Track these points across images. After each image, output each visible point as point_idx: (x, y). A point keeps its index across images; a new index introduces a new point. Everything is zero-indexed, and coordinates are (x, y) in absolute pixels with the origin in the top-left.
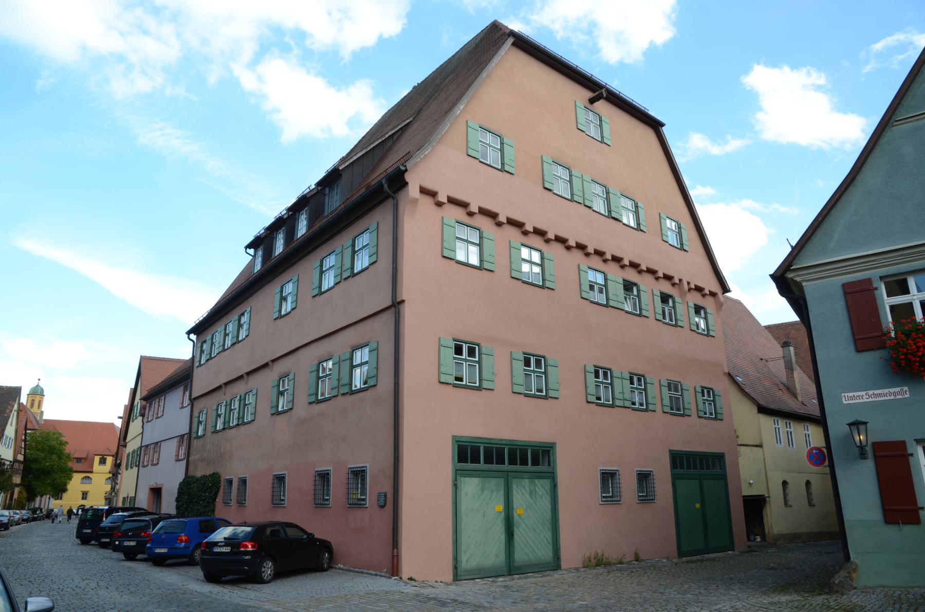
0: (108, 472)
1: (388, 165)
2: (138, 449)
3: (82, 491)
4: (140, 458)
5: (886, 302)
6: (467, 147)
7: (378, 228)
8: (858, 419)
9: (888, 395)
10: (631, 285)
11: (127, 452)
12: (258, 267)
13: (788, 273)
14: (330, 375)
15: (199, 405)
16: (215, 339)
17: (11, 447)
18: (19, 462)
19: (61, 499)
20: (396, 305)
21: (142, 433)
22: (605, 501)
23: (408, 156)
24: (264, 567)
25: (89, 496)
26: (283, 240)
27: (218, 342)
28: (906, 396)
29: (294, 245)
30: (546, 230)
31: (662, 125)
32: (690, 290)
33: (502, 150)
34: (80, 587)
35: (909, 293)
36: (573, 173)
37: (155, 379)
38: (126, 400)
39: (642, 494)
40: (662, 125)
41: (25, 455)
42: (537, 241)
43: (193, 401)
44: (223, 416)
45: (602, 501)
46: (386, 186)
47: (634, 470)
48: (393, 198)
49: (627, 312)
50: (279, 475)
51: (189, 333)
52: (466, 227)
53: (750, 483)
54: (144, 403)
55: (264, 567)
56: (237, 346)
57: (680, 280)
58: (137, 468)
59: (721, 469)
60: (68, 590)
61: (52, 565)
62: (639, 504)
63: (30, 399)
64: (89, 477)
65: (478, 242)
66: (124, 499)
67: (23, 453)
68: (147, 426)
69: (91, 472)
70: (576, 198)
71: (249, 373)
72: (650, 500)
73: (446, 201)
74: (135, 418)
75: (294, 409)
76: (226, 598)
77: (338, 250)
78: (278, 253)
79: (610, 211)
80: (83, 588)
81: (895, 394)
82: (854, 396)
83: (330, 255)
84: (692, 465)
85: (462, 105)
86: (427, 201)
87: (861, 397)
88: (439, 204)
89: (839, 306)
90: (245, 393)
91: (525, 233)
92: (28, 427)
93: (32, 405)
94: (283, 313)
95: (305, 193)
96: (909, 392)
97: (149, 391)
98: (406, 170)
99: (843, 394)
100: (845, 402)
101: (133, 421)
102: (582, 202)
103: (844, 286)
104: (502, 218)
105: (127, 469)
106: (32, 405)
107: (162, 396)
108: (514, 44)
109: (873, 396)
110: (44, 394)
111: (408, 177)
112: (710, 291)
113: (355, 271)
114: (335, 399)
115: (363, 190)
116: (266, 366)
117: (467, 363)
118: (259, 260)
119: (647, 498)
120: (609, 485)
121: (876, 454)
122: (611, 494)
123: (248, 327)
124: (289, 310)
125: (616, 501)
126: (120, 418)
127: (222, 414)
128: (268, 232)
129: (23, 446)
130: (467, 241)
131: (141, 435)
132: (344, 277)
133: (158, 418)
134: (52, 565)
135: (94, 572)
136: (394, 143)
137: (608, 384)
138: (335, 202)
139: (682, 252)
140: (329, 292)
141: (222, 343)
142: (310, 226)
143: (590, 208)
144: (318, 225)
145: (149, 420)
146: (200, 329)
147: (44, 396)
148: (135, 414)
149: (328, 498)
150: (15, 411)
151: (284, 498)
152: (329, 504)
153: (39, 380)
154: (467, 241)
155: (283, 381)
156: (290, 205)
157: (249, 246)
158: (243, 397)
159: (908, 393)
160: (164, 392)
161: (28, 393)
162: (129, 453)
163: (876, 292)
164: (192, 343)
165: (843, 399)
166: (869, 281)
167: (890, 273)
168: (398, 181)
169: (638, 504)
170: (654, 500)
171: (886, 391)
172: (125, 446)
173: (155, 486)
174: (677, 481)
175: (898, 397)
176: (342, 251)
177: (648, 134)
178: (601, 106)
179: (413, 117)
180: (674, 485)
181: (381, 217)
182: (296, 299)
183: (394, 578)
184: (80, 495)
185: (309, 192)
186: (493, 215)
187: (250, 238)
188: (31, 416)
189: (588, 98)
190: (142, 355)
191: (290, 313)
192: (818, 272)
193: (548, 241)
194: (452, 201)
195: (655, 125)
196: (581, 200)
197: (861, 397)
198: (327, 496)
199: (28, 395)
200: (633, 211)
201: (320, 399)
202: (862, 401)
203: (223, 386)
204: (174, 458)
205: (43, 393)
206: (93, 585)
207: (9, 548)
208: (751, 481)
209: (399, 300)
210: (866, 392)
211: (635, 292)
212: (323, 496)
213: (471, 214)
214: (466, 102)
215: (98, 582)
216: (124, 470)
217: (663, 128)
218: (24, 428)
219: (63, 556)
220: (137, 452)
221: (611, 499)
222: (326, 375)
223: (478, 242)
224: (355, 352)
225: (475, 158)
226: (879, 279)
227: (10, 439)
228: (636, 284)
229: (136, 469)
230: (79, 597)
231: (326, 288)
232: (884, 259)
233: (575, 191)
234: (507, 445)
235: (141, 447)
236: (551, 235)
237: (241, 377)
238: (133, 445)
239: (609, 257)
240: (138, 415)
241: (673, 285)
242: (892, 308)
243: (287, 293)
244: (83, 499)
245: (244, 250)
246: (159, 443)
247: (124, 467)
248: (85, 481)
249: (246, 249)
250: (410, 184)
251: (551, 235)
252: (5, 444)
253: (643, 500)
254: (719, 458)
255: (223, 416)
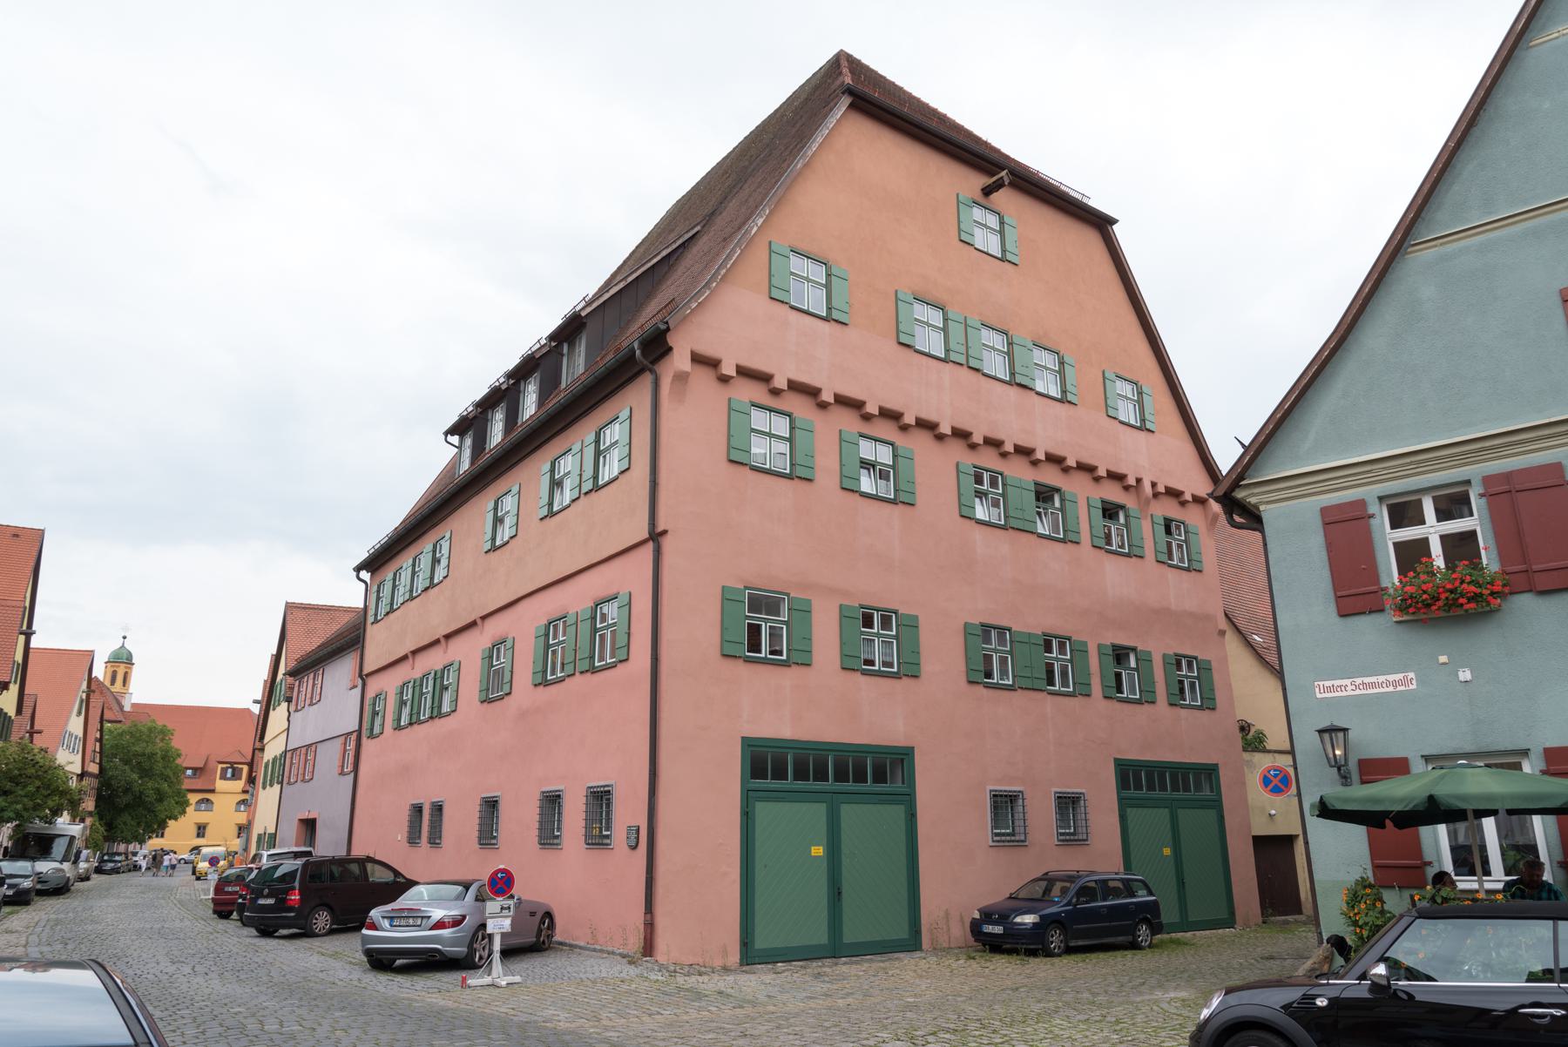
0: (240, 790)
1: (647, 317)
2: (281, 755)
3: (196, 823)
4: (284, 769)
5: (1388, 537)
6: (770, 285)
7: (631, 417)
8: (1335, 724)
9: (1384, 685)
10: (1049, 491)
11: (265, 760)
12: (465, 465)
13: (1237, 490)
14: (614, 624)
15: (374, 686)
16: (419, 566)
17: (78, 751)
18: (91, 775)
19: (162, 836)
20: (656, 536)
21: (288, 729)
22: (998, 841)
23: (672, 307)
24: (316, 919)
25: (209, 831)
26: (469, 450)
27: (403, 584)
28: (1411, 687)
29: (485, 459)
30: (901, 410)
31: (1113, 221)
32: (1156, 495)
33: (828, 286)
34: (167, 973)
35: (1424, 523)
36: (950, 315)
37: (306, 643)
38: (264, 673)
39: (1063, 831)
40: (1113, 221)
41: (100, 764)
42: (886, 429)
43: (364, 677)
44: (409, 703)
45: (993, 841)
46: (638, 352)
47: (1051, 791)
48: (651, 371)
49: (1041, 536)
50: (489, 798)
51: (358, 569)
52: (768, 412)
53: (1270, 814)
54: (290, 680)
55: (316, 919)
56: (432, 592)
57: (1139, 481)
58: (279, 786)
59: (1212, 791)
60: (149, 976)
61: (132, 941)
62: (1061, 847)
63: (110, 670)
64: (208, 800)
65: (788, 436)
66: (259, 835)
67: (98, 761)
68: (296, 717)
69: (213, 791)
70: (953, 357)
71: (448, 637)
72: (1080, 840)
73: (734, 374)
74: (276, 704)
75: (513, 693)
76: (381, 988)
77: (576, 447)
78: (528, 417)
79: (1013, 374)
80: (170, 974)
81: (1395, 684)
82: (1333, 686)
83: (564, 454)
84: (1180, 782)
85: (762, 217)
86: (703, 377)
87: (1343, 688)
88: (724, 380)
89: (1315, 543)
90: (401, 684)
91: (867, 418)
92: (105, 717)
93: (113, 682)
94: (498, 543)
95: (533, 350)
96: (1417, 681)
97: (299, 661)
98: (668, 329)
99: (1316, 683)
100: (1319, 696)
101: (274, 709)
102: (964, 362)
103: (1325, 511)
104: (827, 396)
105: (264, 788)
106: (113, 682)
107: (318, 670)
108: (852, 106)
109: (1361, 687)
110: (133, 661)
111: (672, 340)
112: (1193, 496)
113: (600, 483)
114: (571, 678)
115: (611, 356)
116: (473, 624)
117: (768, 624)
118: (467, 453)
119: (1013, 838)
120: (1008, 817)
121: (1363, 777)
122: (1072, 831)
123: (515, 521)
124: (567, 501)
125: (1018, 841)
126: (256, 702)
127: (408, 700)
128: (479, 410)
129: (98, 749)
130: (770, 435)
131: (286, 733)
132: (584, 490)
133: (311, 704)
134: (132, 941)
135: (193, 952)
136: (671, 267)
137: (1006, 652)
138: (576, 367)
139: (1143, 434)
140: (562, 513)
141: (408, 588)
142: (541, 402)
143: (977, 370)
144: (553, 402)
145: (299, 708)
146: (376, 562)
147: (133, 664)
148: (277, 698)
149: (609, 833)
150: (83, 692)
151: (559, 833)
152: (610, 844)
153: (125, 638)
154: (770, 435)
155: (498, 649)
156: (511, 367)
157: (452, 431)
158: (439, 675)
159: (1414, 682)
160: (316, 665)
161: (107, 660)
162: (269, 761)
163: (1372, 521)
164: (363, 585)
165: (1317, 690)
166: (1361, 504)
167: (1393, 492)
168: (657, 345)
169: (991, 849)
170: (1087, 840)
171: (1382, 679)
172: (262, 750)
173: (305, 816)
174: (1129, 810)
175: (1399, 688)
176: (581, 450)
177: (1091, 238)
178: (1005, 198)
179: (702, 224)
180: (1123, 818)
181: (636, 398)
182: (628, 452)
183: (645, 959)
184: (194, 831)
185: (539, 349)
186: (812, 392)
187: (453, 419)
188: (111, 699)
189: (980, 188)
190: (289, 601)
191: (616, 479)
192: (1283, 489)
193: (904, 428)
194: (743, 372)
195: (1101, 224)
196: (962, 359)
197: (1343, 688)
198: (558, 831)
199: (106, 663)
200: (1055, 371)
201: (599, 666)
202: (1344, 694)
203: (443, 640)
204: (336, 770)
205: (131, 660)
206: (187, 969)
207: (71, 914)
208: (1273, 812)
209: (660, 528)
210: (1351, 680)
211: (1057, 504)
212: (601, 831)
213: (776, 392)
214: (768, 211)
215: (194, 967)
216: (261, 789)
217: (1114, 227)
218: (98, 719)
219: (151, 928)
220: (280, 759)
221: (1072, 837)
222: (559, 642)
223: (788, 436)
224: (599, 607)
225: (782, 302)
226: (1377, 500)
227: (76, 738)
228: (1058, 490)
229: (277, 787)
230: (162, 985)
231: (606, 479)
232: (1385, 468)
233: (952, 346)
234: (870, 752)
235: (286, 751)
236: (909, 419)
237: (436, 642)
238: (273, 749)
239: (1009, 447)
240: (282, 699)
241: (1127, 488)
242: (1398, 546)
243: (562, 473)
244: (198, 836)
245: (443, 437)
246: (313, 748)
247: (261, 785)
248: (203, 806)
249: (446, 436)
250: (675, 350)
251: (909, 419)
252: (68, 747)
253: (1067, 841)
254: (1208, 773)
255: (409, 703)
